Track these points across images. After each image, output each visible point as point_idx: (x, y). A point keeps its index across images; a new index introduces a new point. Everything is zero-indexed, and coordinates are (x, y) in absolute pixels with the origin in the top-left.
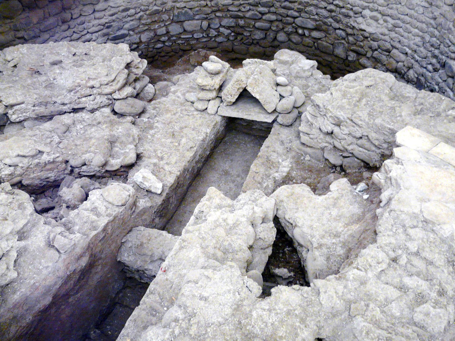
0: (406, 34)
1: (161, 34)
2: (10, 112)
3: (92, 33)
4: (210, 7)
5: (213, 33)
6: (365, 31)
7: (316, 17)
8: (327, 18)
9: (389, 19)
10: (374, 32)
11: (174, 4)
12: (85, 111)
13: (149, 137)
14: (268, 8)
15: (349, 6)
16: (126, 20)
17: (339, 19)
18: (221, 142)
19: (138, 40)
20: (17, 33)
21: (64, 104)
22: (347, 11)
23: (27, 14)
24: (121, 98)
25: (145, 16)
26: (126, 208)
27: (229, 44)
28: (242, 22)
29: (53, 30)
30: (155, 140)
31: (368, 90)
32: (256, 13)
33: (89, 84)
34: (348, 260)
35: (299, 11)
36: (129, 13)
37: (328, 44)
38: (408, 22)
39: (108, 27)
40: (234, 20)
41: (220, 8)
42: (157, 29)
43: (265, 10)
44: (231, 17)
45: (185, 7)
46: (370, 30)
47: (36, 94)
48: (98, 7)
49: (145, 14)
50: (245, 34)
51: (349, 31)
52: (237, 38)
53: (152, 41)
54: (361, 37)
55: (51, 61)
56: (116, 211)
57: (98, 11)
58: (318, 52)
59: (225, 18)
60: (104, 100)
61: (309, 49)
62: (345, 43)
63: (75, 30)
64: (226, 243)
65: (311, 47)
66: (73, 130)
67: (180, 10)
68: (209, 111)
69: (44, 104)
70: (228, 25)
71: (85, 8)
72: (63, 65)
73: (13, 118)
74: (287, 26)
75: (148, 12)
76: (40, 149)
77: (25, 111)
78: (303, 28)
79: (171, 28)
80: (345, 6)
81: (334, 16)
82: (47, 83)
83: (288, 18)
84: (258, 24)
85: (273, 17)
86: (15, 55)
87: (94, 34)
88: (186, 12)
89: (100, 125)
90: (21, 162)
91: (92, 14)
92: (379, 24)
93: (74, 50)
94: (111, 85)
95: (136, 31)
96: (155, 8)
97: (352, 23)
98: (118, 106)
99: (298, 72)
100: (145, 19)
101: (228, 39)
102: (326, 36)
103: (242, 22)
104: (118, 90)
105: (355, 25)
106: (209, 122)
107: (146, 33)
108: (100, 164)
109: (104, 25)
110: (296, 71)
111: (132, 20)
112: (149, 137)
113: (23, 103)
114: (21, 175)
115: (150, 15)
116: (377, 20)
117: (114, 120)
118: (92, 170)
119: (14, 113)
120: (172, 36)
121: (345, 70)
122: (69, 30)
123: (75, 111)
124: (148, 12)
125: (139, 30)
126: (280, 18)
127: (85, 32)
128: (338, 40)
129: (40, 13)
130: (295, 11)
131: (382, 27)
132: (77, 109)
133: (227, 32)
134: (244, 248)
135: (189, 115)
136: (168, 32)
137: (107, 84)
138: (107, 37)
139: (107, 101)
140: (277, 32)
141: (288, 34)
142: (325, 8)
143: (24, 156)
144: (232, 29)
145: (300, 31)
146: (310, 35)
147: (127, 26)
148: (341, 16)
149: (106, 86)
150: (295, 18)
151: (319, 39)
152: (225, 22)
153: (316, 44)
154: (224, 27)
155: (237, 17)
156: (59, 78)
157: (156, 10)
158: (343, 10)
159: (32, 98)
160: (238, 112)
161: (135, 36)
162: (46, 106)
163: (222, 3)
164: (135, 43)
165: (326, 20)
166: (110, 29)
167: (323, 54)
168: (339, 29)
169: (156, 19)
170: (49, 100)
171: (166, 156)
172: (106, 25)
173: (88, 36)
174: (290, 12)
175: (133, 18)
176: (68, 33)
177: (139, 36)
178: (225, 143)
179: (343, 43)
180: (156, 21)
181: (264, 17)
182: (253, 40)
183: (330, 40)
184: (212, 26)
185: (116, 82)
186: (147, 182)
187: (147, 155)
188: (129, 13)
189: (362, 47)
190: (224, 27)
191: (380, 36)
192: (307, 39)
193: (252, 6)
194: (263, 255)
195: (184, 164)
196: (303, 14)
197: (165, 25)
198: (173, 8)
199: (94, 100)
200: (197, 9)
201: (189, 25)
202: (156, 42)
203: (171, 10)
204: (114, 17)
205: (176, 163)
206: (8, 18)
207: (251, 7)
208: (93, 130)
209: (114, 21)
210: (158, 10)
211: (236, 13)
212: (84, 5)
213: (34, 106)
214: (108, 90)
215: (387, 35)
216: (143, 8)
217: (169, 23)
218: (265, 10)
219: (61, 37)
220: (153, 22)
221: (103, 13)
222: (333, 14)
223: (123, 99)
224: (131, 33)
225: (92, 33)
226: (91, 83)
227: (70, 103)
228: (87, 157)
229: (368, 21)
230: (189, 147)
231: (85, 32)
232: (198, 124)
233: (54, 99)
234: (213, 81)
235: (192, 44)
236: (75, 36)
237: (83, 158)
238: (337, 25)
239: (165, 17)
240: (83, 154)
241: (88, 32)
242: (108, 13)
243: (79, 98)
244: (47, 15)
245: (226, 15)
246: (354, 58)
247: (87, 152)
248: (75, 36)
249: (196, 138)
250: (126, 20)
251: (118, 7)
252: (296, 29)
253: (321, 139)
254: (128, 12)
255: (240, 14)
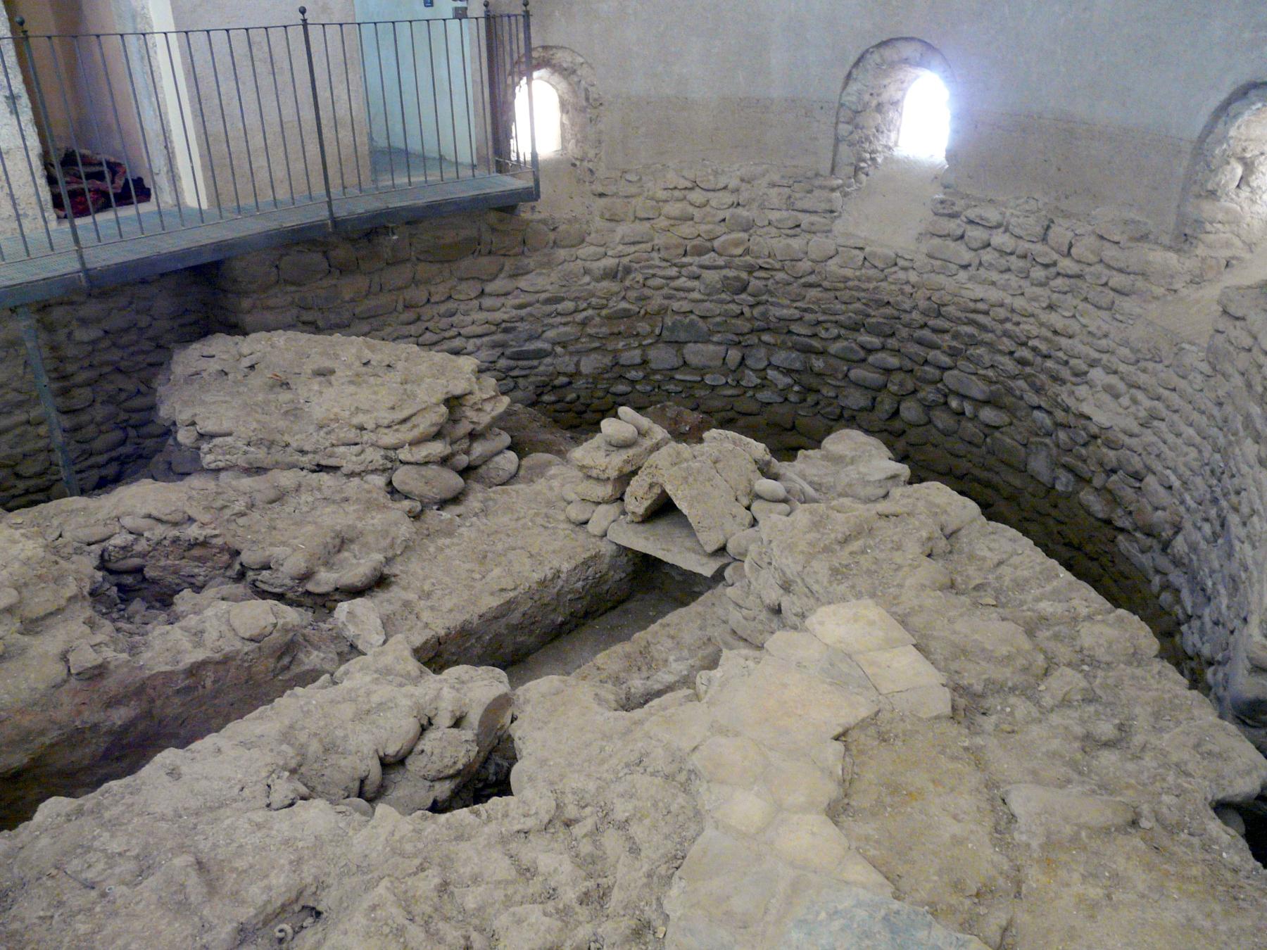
0: (1171, 438)
1: (628, 363)
2: (205, 447)
3: (468, 337)
4: (748, 320)
5: (751, 379)
6: (1089, 419)
7: (990, 373)
8: (1015, 377)
9: (1140, 396)
10: (1107, 424)
11: (666, 302)
12: (339, 473)
13: (432, 549)
14: (882, 339)
15: (1060, 354)
16: (551, 321)
17: (1038, 383)
18: (614, 608)
19: (571, 369)
20: (304, 312)
21: (302, 452)
22: (1056, 366)
23: (334, 282)
24: (412, 460)
25: (598, 319)
26: (260, 648)
27: (785, 409)
28: (818, 364)
29: (381, 318)
30: (440, 557)
31: (882, 523)
32: (853, 345)
33: (355, 421)
34: (168, 627)
35: (954, 353)
36: (560, 307)
37: (1015, 444)
38: (1176, 407)
39: (506, 331)
40: (802, 356)
41: (772, 326)
42: (621, 351)
43: (876, 341)
44: (794, 348)
45: (691, 312)
46: (1100, 418)
47: (258, 422)
48: (489, 288)
49: (599, 315)
50: (825, 391)
51: (1060, 415)
52: (805, 400)
53: (606, 376)
54: (1083, 433)
55: (315, 367)
56: (232, 645)
57: (491, 295)
58: (991, 461)
59: (780, 348)
60: (375, 457)
61: (975, 450)
62: (1052, 445)
63: (430, 325)
64: (340, 733)
65: (978, 447)
66: (292, 502)
67: (678, 317)
68: (589, 526)
69: (267, 443)
70: (786, 365)
71: (464, 286)
72: (333, 378)
73: (207, 460)
74: (924, 386)
75: (604, 312)
76: (190, 512)
77: (230, 450)
78: (963, 397)
79: (652, 354)
80: (1053, 353)
81: (1030, 375)
82: (290, 406)
83: (927, 368)
84: (856, 373)
85: (894, 362)
86: (259, 347)
87: (472, 341)
88: (692, 323)
89: (345, 505)
90: (150, 529)
91: (476, 298)
92: (1120, 406)
93: (367, 354)
94: (397, 430)
95: (571, 348)
96: (624, 305)
97: (1064, 396)
98: (401, 477)
99: (850, 485)
100: (595, 326)
101: (786, 399)
102: (1011, 424)
103: (818, 364)
104: (410, 444)
105: (1070, 402)
106: (579, 550)
107: (593, 356)
108: (294, 572)
109: (498, 325)
110: (847, 480)
111: (565, 324)
112: (432, 549)
113: (229, 434)
114: (143, 555)
115: (609, 318)
116: (1117, 396)
117: (376, 499)
118: (278, 582)
119: (210, 451)
120: (655, 372)
121: (1049, 515)
122: (419, 323)
123: (320, 468)
124: (604, 312)
125: (579, 346)
126: (908, 364)
127: (453, 332)
128: (1037, 435)
129: (361, 282)
130: (944, 352)
131: (1127, 416)
132: (326, 467)
133: (783, 381)
134: (366, 751)
135: (546, 528)
136: (645, 362)
137: (389, 427)
138: (500, 350)
139: (381, 462)
140: (901, 398)
141: (928, 407)
142: (1011, 353)
143: (159, 520)
144: (796, 376)
145: (954, 404)
146: (976, 416)
147: (551, 334)
148: (1043, 377)
149: (386, 431)
150: (944, 369)
151: (997, 428)
152: (780, 357)
153: (988, 440)
154: (777, 368)
155: (807, 350)
156: (315, 400)
157: (625, 310)
158: (1049, 364)
159: (247, 428)
160: (647, 539)
161: (567, 358)
162: (269, 448)
163: (777, 314)
164: (565, 374)
165: (1011, 383)
166: (511, 336)
167: (1004, 468)
168: (1039, 408)
169: (622, 328)
170: (278, 437)
171: (439, 592)
172: (504, 325)
173: (457, 343)
174: (932, 355)
175: (569, 319)
176: (413, 329)
177: (575, 359)
178: (626, 612)
179: (1046, 445)
180: (620, 333)
181: (871, 359)
182: (843, 408)
183: (1020, 433)
184: (749, 362)
185: (409, 425)
186: (356, 625)
187: (403, 583)
188: (560, 307)
189: (1084, 461)
190: (777, 368)
191: (1121, 436)
192: (970, 425)
193: (845, 328)
194: (423, 793)
195: (467, 617)
196: (961, 363)
197: (640, 345)
198: (662, 311)
199: (358, 455)
200: (718, 319)
201: (697, 353)
202: (616, 379)
203: (658, 313)
204: (523, 312)
205: (451, 611)
206: (293, 284)
207: (843, 332)
208: (328, 510)
209: (522, 319)
210: (629, 310)
211: (806, 339)
212: (461, 279)
213: (249, 444)
214: (389, 438)
215: (1137, 436)
216: (594, 301)
217: (650, 341)
218: (876, 341)
219: (396, 335)
220: (612, 334)
221: (502, 300)
222: (1028, 370)
223: (417, 464)
224: (559, 349)
225: (468, 337)
226: (360, 419)
227: (315, 452)
228: (278, 551)
229: (1098, 395)
230: (496, 587)
231: (453, 332)
232: (551, 548)
233: (287, 438)
234: (608, 459)
235: (701, 397)
236: (428, 337)
237: (267, 553)
238: (1035, 400)
239: (643, 327)
240: (271, 544)
241: (460, 334)
242: (511, 301)
243: (333, 445)
244: (375, 288)
245: (784, 342)
246: (1067, 486)
247: (284, 543)
248: (428, 337)
249: (526, 574)
250: (551, 321)
251: (537, 292)
252: (946, 396)
253: (761, 622)
254: (555, 306)
255: (815, 343)
